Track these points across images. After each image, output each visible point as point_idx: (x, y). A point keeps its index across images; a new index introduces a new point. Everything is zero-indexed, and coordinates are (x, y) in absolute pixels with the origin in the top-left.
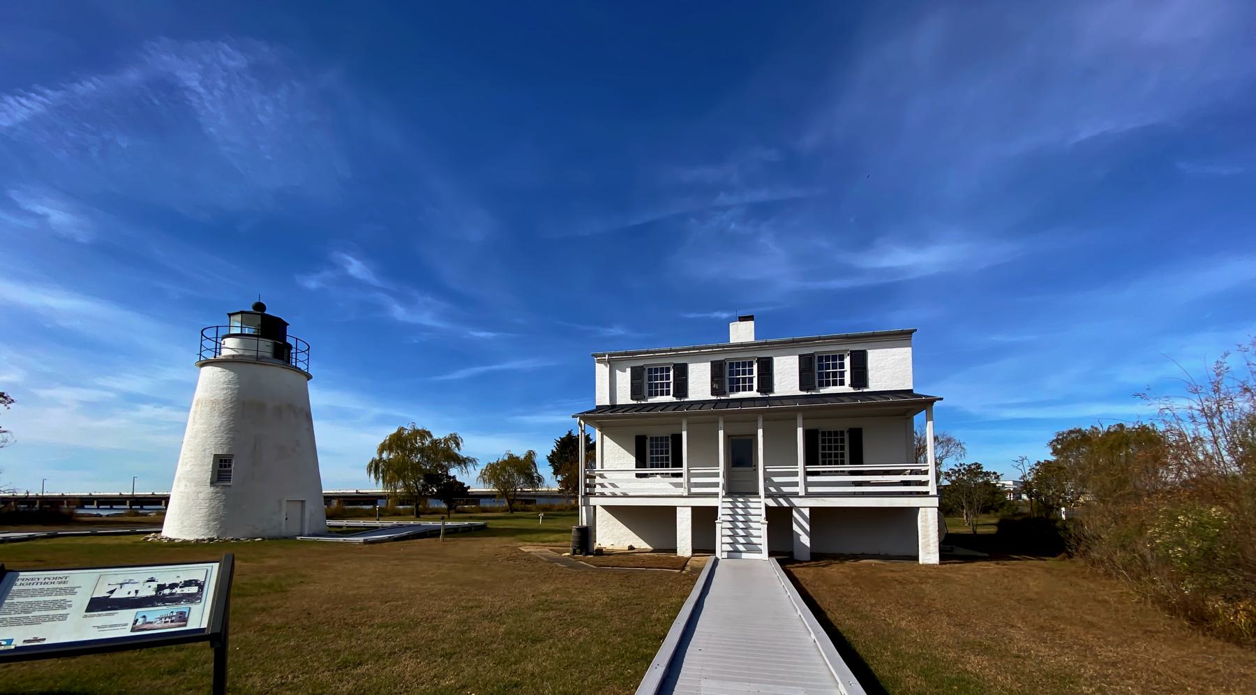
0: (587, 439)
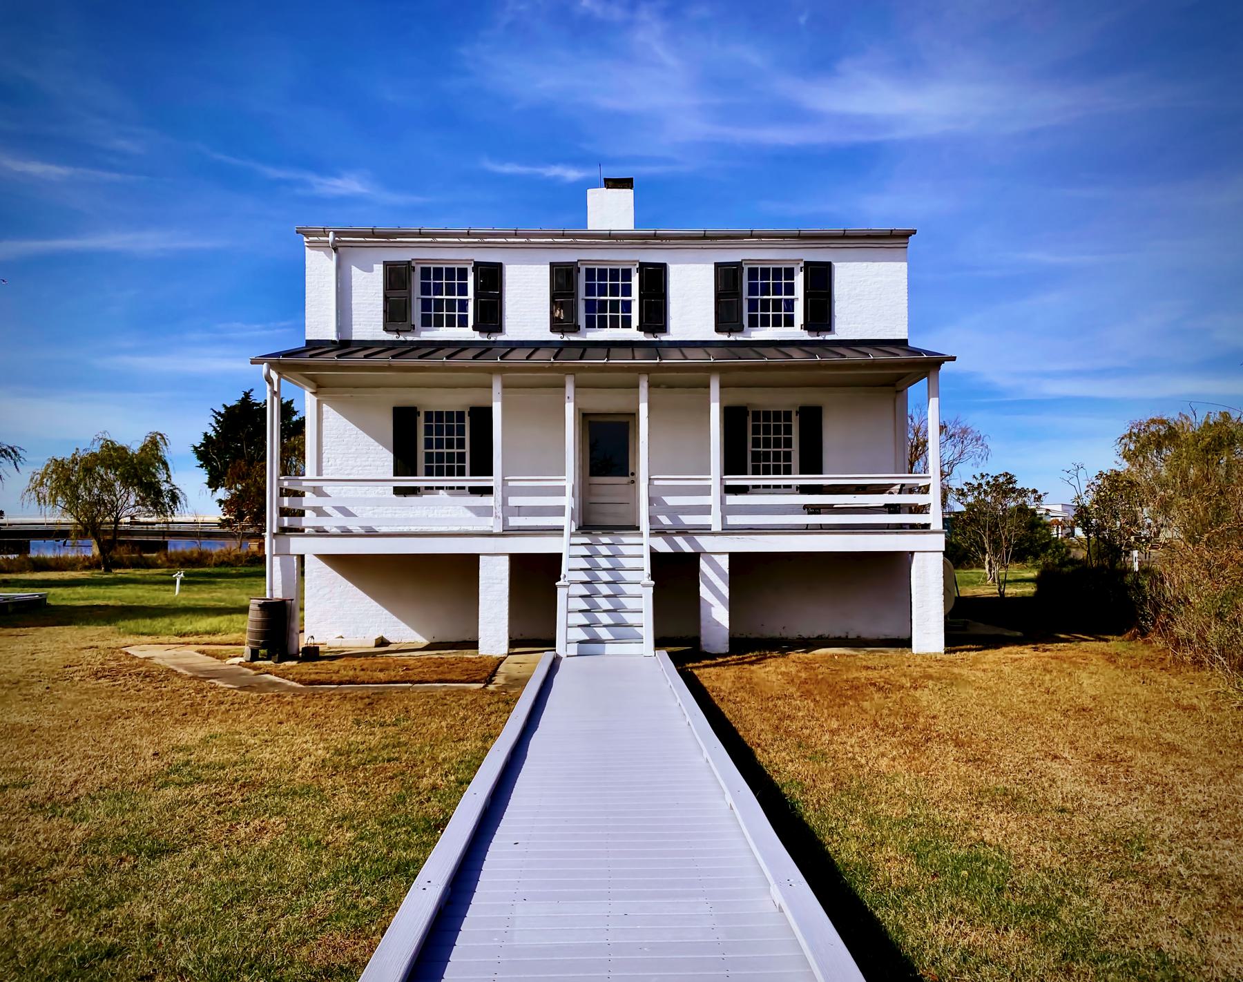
0: (287, 410)
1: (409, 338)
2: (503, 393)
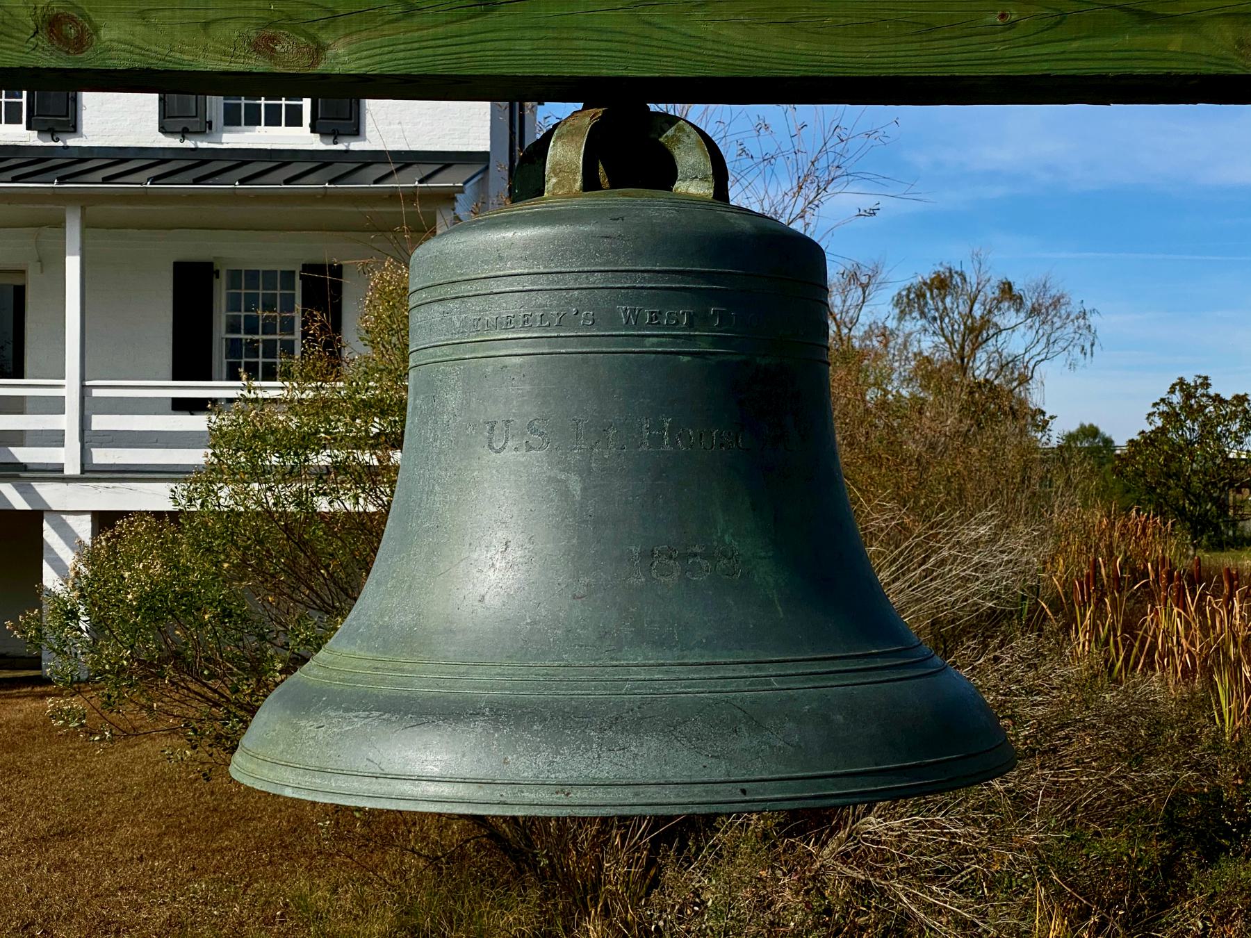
1: (203, 145)
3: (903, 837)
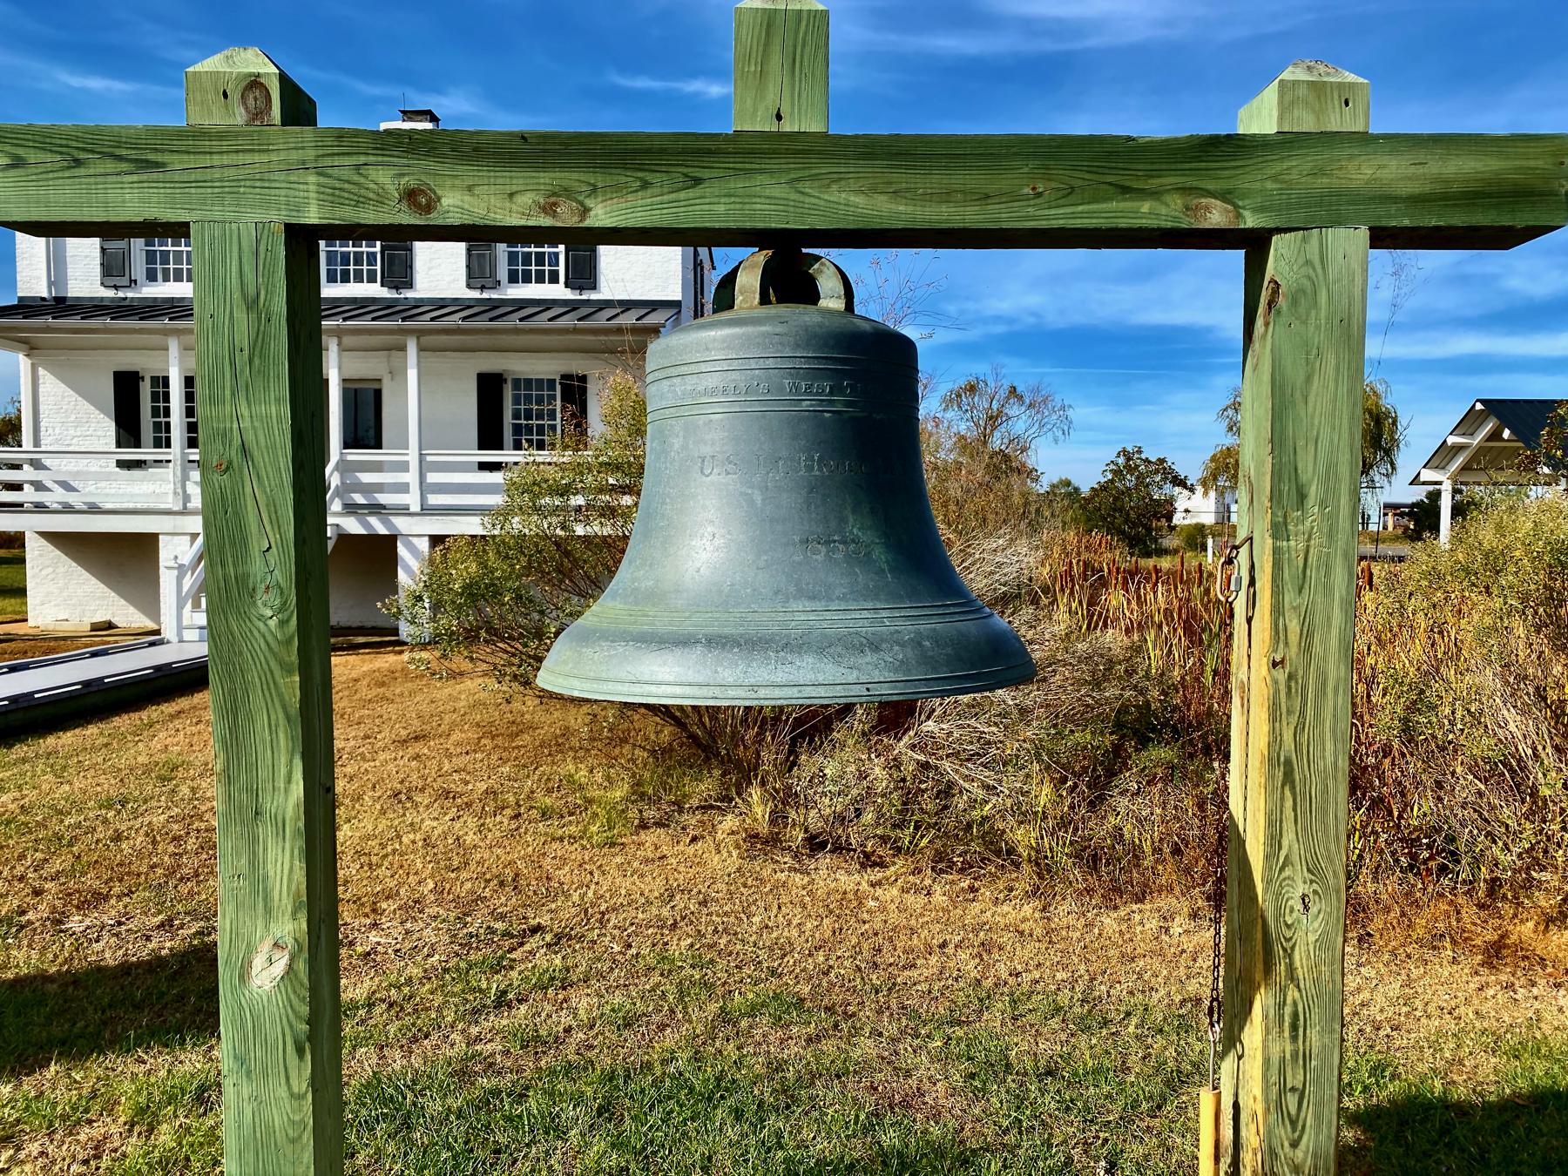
1: (130, 295)
2: (419, 356)
3: (950, 734)
